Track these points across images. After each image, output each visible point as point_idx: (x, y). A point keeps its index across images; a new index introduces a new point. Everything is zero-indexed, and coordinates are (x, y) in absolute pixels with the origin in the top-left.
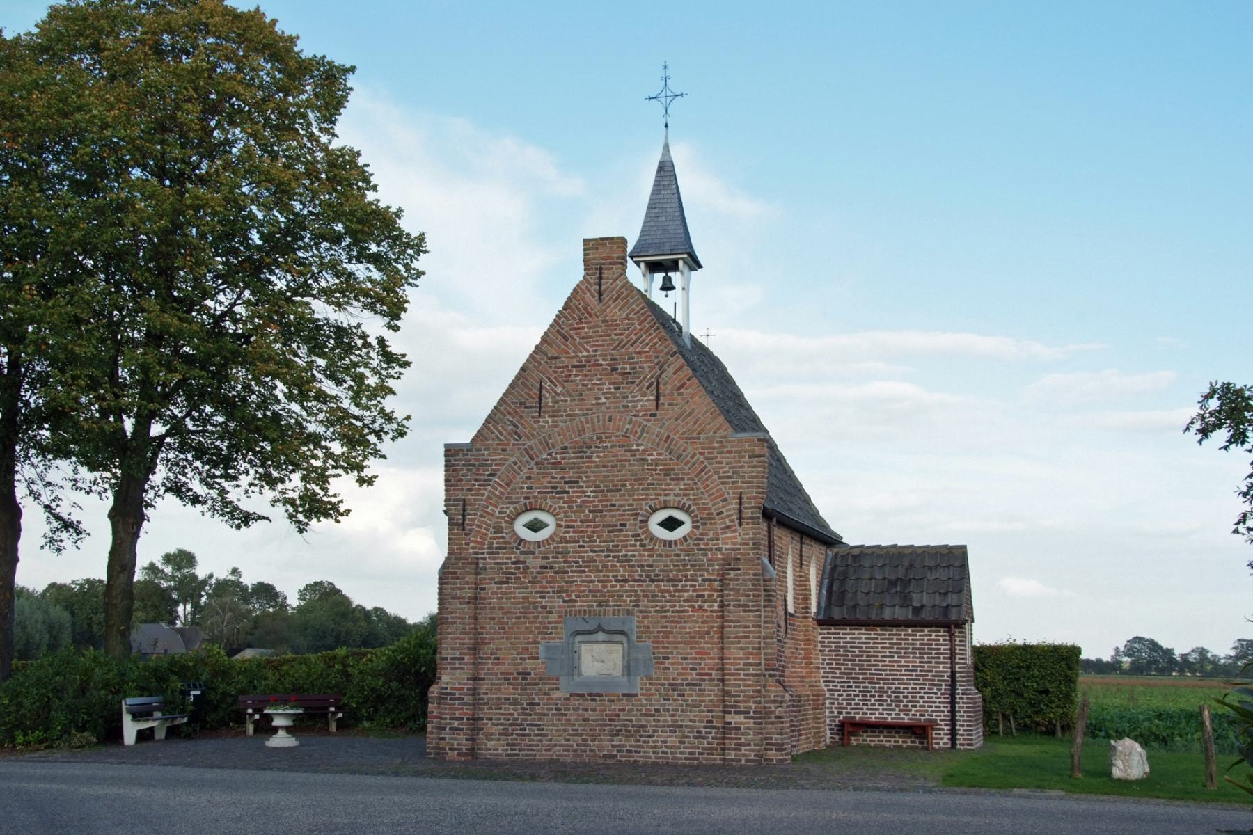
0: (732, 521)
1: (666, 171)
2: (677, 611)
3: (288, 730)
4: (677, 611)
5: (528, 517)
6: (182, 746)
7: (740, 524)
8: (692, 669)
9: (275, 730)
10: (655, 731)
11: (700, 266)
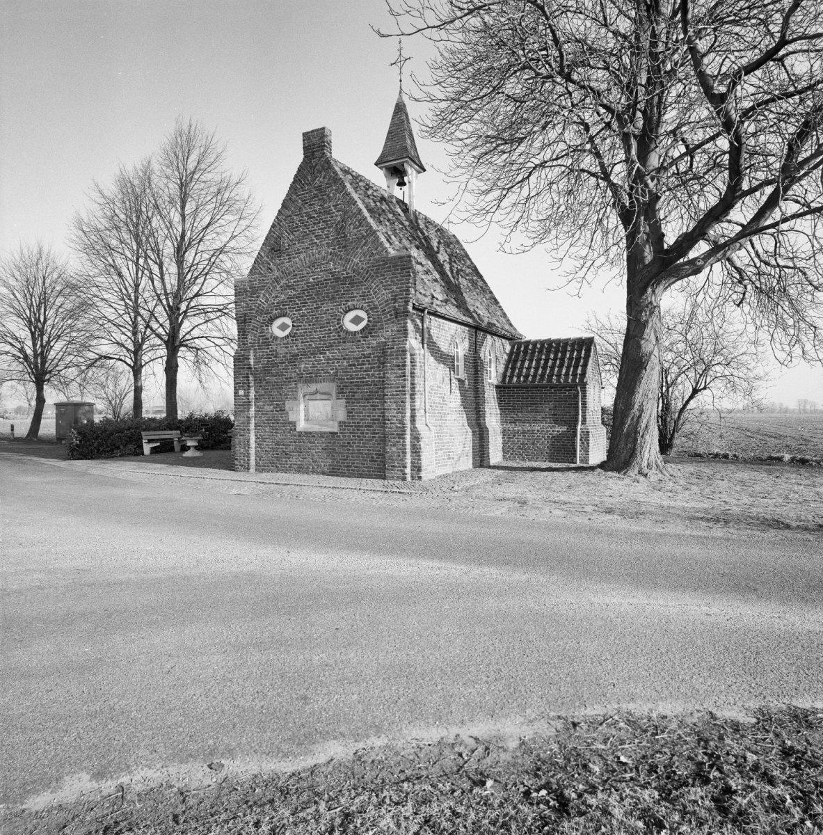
0: (391, 315)
1: (400, 109)
2: (359, 378)
3: (196, 448)
4: (359, 378)
5: (351, 315)
6: (158, 456)
7: (396, 317)
8: (369, 416)
9: (189, 448)
10: (347, 457)
11: (425, 170)
